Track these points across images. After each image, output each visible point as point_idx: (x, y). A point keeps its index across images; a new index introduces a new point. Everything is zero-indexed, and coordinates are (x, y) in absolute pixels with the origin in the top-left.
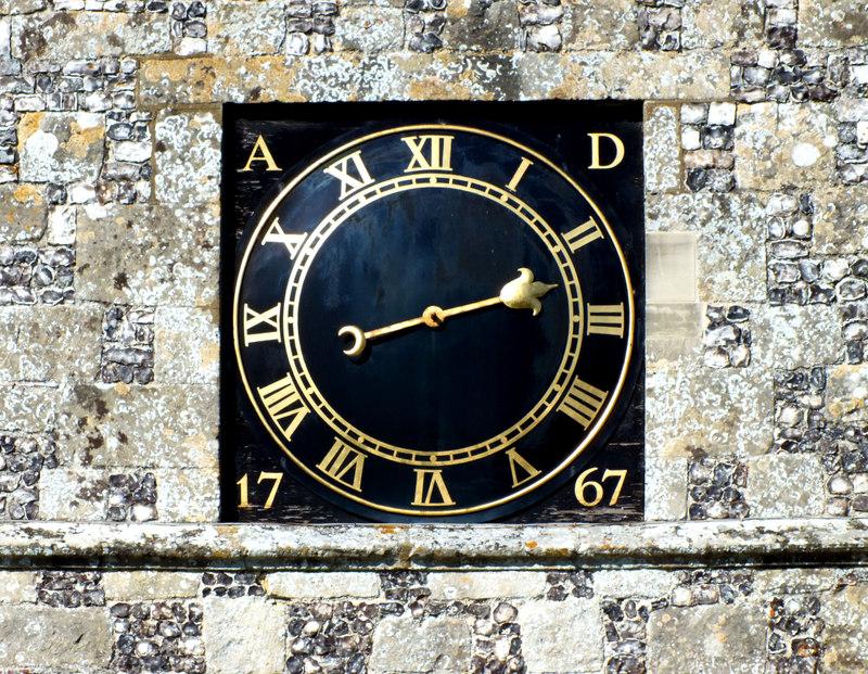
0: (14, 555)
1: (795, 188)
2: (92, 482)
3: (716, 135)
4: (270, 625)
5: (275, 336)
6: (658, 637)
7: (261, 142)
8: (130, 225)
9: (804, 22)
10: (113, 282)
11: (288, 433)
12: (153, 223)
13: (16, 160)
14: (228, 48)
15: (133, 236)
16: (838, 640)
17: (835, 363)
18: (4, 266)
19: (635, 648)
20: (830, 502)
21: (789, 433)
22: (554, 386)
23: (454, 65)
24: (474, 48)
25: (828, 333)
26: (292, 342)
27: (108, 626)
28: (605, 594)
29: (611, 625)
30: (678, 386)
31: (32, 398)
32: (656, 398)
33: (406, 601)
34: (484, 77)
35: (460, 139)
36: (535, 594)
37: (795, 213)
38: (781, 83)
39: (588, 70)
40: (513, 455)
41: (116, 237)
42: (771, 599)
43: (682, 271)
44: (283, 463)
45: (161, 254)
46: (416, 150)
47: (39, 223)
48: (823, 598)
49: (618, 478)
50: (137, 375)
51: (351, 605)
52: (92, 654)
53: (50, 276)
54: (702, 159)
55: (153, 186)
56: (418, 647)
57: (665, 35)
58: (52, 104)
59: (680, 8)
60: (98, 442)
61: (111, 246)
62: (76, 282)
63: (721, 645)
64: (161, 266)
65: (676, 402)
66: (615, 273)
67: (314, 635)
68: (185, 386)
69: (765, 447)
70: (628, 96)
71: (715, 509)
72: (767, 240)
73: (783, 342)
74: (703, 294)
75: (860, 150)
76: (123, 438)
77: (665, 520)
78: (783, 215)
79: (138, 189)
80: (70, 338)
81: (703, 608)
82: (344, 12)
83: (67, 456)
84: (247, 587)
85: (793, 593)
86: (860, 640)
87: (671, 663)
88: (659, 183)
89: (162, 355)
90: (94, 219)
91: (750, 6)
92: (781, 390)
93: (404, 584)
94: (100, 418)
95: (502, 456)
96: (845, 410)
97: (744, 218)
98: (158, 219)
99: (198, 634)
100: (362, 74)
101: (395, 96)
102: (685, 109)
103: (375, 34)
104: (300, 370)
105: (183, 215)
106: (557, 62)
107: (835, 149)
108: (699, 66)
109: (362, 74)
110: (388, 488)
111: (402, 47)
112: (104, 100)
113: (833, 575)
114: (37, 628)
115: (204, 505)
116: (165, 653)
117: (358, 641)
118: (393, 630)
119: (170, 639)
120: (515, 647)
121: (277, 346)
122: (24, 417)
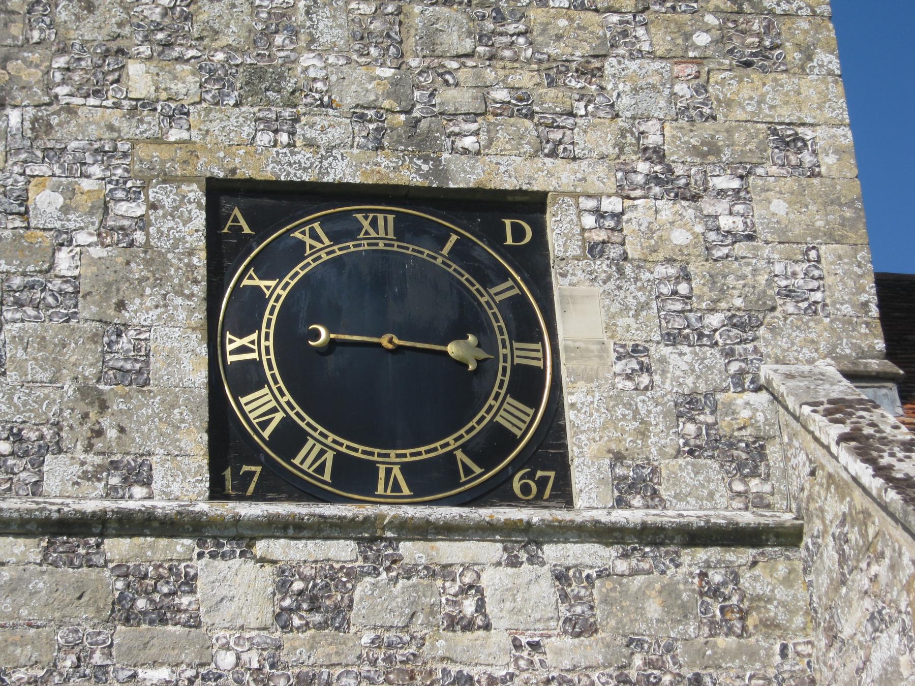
0: (22, 518)
1: (675, 260)
2: (93, 465)
3: (609, 219)
4: (259, 584)
5: (255, 356)
6: (605, 600)
7: (236, 212)
8: (128, 263)
9: (669, 144)
10: (113, 306)
11: (266, 434)
12: (148, 263)
13: (27, 212)
14: (208, 138)
15: (131, 272)
16: (758, 607)
17: (722, 391)
18: (16, 292)
19: (586, 609)
20: (732, 499)
21: (692, 442)
22: (491, 401)
23: (394, 160)
24: (410, 149)
25: (714, 367)
26: (269, 361)
27: (108, 584)
28: (554, 563)
29: (563, 589)
30: (596, 403)
31: (39, 396)
32: (579, 411)
33: (382, 565)
34: (420, 169)
35: (399, 217)
36: (494, 560)
37: (677, 278)
38: (656, 185)
39: (502, 169)
40: (459, 455)
41: (115, 272)
42: (698, 571)
43: (585, 317)
44: (263, 459)
45: (155, 287)
46: (366, 224)
47: (47, 259)
48: (740, 572)
49: (549, 477)
50: (135, 379)
51: (332, 567)
52: (92, 609)
53: (57, 300)
54: (599, 236)
55: (148, 235)
56: (394, 604)
57: (561, 147)
58: (58, 172)
59: (572, 129)
60: (99, 433)
61: (111, 279)
62: (80, 306)
63: (659, 609)
64: (155, 295)
65: (596, 415)
66: (531, 319)
67: (301, 593)
68: (177, 389)
69: (672, 452)
70: (535, 188)
71: (637, 501)
72: (657, 297)
73: (678, 373)
74: (609, 334)
75: (723, 236)
76: (122, 430)
77: (591, 499)
78: (668, 278)
79: (135, 236)
80: (74, 349)
81: (640, 579)
82: (304, 119)
83: (70, 443)
84: (238, 551)
85: (715, 567)
86: (776, 607)
87: (617, 623)
88: (566, 252)
89: (156, 363)
90: (96, 257)
91: (627, 131)
92: (682, 409)
93: (379, 550)
94: (101, 413)
95: (451, 456)
96: (736, 427)
97: (637, 279)
98: (152, 259)
99: (193, 591)
100: (321, 162)
101: (348, 179)
102: (581, 200)
103: (329, 135)
104: (276, 382)
105: (174, 258)
106: (477, 161)
107: (703, 234)
108: (590, 170)
109: (321, 162)
110: (354, 478)
111: (352, 146)
112: (103, 170)
113: (746, 555)
114: (41, 585)
115: (195, 486)
116: (161, 608)
117: (339, 598)
118: (370, 589)
119: (166, 595)
120: (481, 607)
121: (258, 364)
122: (31, 411)
